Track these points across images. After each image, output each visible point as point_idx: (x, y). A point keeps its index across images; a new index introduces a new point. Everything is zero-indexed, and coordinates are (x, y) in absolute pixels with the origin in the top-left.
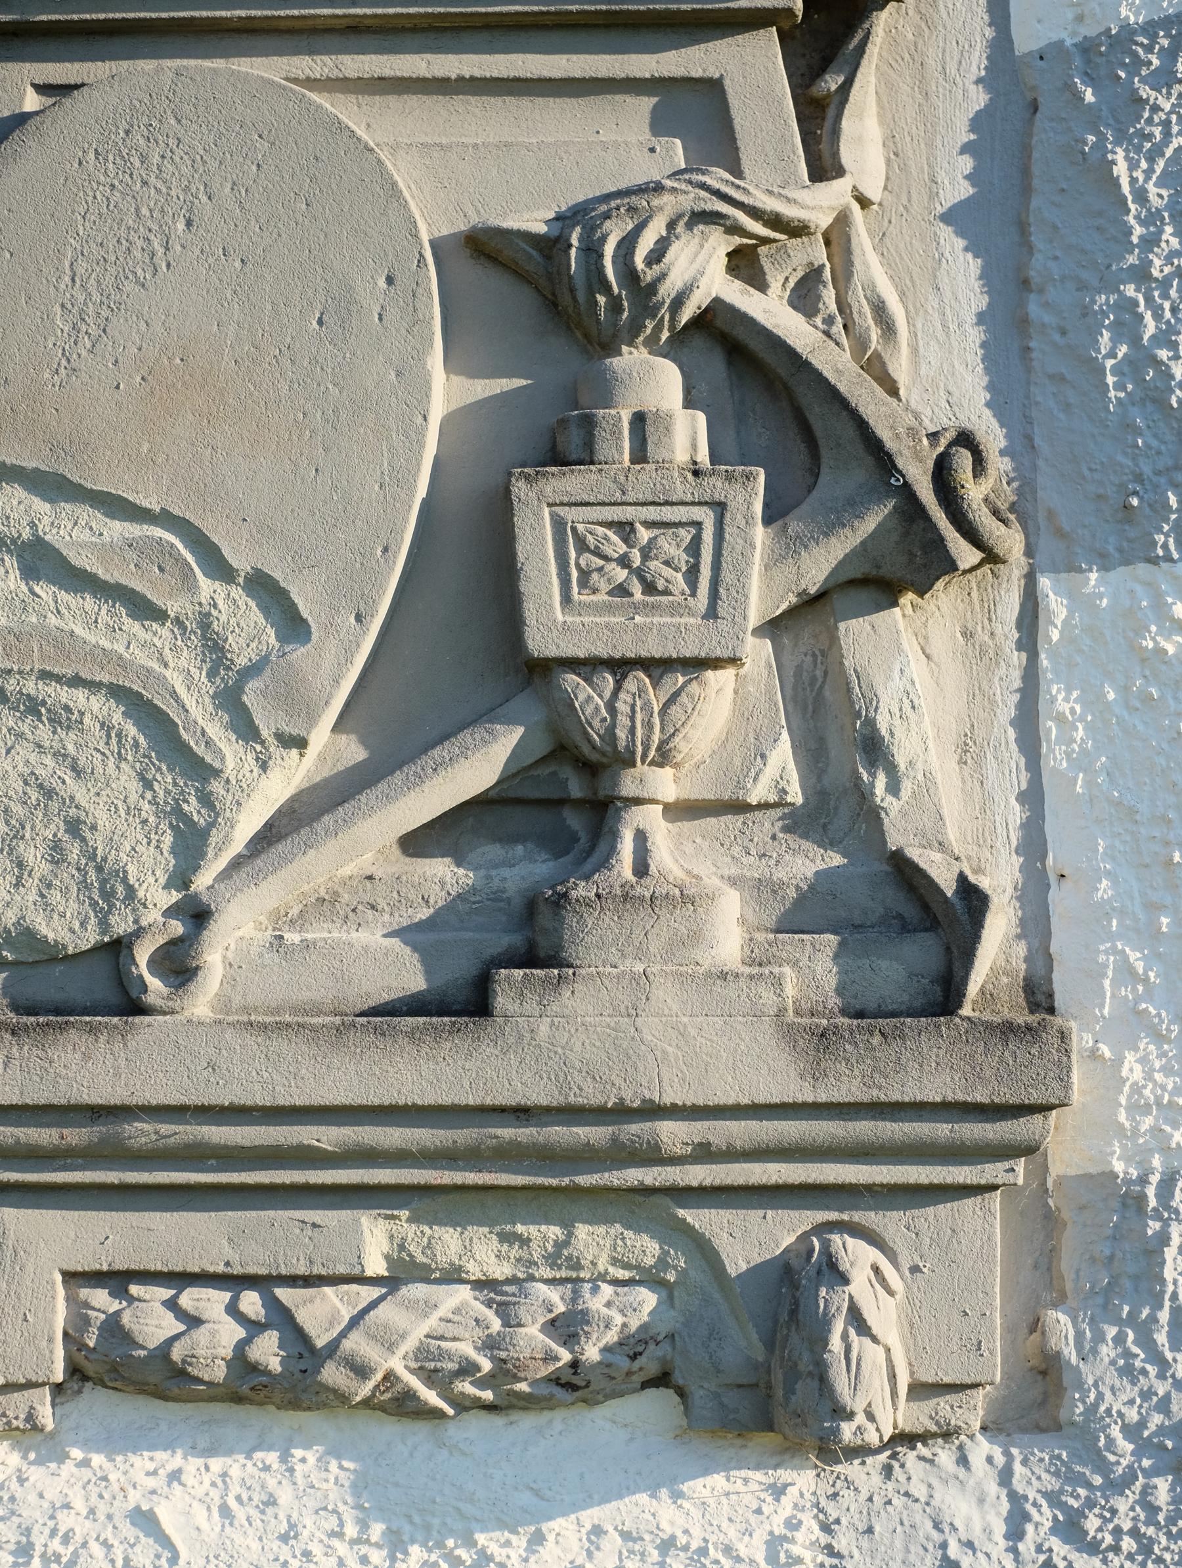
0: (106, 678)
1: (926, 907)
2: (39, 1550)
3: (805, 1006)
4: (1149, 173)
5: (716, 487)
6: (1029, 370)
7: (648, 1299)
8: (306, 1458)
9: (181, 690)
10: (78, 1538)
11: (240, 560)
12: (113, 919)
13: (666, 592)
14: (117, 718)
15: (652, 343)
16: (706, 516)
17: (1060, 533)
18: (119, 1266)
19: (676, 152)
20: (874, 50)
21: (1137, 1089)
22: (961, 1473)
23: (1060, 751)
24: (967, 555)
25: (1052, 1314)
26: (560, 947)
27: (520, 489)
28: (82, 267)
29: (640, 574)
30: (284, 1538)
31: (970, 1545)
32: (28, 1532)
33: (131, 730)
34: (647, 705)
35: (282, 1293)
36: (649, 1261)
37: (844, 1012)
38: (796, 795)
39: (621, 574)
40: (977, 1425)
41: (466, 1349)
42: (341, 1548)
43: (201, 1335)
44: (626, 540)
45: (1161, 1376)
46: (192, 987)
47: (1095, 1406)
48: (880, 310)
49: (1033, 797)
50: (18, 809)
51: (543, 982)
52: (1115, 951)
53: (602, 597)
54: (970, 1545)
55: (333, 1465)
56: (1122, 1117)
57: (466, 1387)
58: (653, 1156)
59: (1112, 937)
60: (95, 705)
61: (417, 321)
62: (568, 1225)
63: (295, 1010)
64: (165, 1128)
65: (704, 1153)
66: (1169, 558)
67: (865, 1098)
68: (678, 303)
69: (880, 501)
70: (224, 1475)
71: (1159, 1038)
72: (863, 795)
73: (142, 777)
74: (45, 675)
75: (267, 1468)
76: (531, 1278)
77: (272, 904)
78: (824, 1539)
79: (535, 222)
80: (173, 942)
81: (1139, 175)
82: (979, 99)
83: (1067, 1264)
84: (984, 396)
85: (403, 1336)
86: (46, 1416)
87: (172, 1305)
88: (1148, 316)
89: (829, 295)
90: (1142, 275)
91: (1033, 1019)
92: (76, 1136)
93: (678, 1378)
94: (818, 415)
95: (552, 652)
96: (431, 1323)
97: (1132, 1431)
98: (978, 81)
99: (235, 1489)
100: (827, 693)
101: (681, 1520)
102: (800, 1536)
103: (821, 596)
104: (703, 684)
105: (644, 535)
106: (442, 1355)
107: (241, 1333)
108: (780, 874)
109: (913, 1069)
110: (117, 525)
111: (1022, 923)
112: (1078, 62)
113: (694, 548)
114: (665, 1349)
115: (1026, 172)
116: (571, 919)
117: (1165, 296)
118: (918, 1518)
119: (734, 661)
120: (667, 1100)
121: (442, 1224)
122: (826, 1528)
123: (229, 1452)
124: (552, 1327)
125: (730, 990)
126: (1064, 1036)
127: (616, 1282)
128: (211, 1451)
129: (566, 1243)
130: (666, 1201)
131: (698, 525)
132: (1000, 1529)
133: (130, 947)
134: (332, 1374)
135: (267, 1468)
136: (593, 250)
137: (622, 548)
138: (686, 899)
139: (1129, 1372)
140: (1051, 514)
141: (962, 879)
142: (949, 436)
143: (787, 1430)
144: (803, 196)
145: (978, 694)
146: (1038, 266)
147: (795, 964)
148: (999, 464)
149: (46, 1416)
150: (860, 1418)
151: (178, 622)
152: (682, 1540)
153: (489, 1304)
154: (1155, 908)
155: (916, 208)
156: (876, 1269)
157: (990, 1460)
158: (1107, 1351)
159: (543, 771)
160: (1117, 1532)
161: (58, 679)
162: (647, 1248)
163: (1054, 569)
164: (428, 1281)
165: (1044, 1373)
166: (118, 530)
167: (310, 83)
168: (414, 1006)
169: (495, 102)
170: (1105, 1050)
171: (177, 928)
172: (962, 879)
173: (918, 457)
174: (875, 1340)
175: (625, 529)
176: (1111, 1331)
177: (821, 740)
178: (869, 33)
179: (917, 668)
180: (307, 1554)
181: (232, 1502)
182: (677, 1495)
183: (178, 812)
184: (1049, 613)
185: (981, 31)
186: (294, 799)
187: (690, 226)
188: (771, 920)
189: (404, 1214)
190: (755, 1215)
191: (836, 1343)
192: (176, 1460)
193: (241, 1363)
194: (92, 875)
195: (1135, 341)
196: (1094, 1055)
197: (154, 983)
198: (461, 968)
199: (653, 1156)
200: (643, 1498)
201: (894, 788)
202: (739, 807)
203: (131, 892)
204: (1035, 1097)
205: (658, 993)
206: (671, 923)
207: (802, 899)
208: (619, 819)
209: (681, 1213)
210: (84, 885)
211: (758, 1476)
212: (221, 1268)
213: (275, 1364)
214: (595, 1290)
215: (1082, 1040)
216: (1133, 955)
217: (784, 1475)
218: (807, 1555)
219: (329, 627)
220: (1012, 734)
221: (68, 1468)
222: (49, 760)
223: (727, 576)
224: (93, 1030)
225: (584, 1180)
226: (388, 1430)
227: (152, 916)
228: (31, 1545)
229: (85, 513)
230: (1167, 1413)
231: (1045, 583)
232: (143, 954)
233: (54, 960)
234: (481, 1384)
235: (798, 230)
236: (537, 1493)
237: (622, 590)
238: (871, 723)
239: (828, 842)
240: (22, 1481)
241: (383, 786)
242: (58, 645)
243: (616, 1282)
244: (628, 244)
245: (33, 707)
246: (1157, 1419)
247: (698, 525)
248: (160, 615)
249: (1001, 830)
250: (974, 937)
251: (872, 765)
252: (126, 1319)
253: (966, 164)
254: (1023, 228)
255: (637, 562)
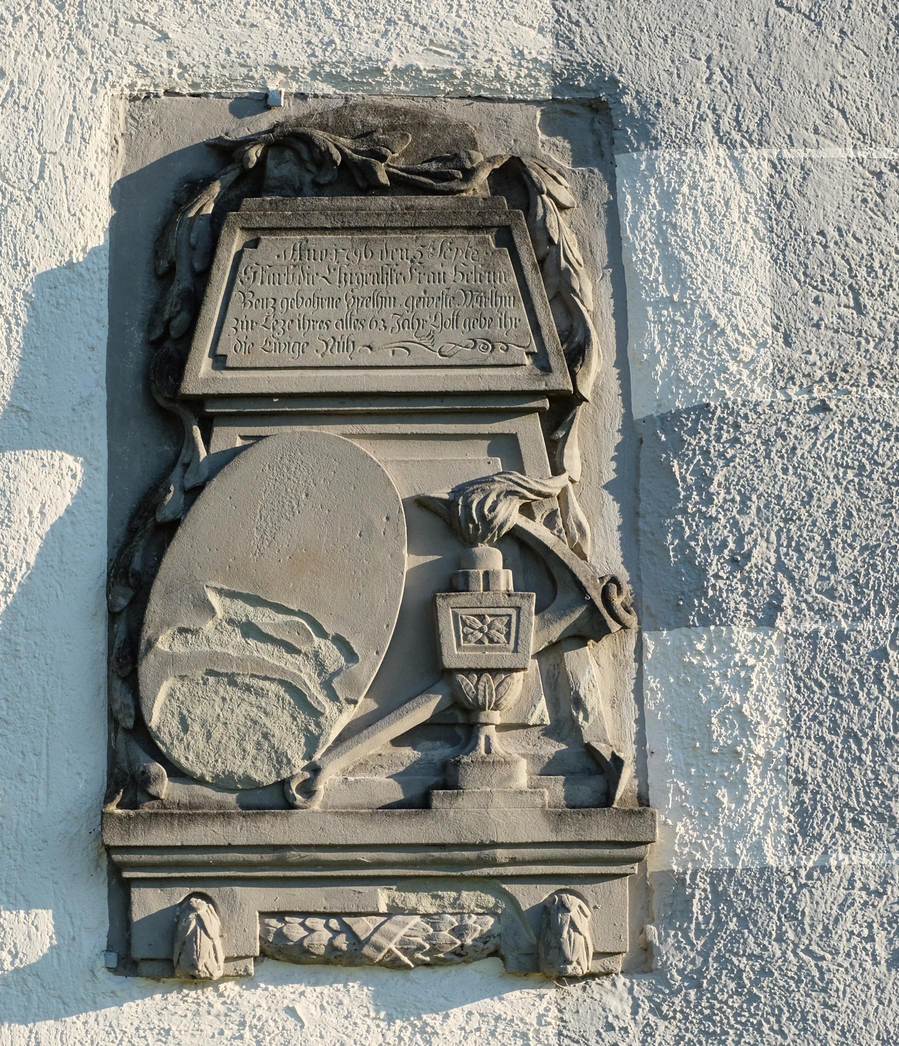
0: (277, 677)
1: (599, 765)
2: (248, 1023)
3: (552, 804)
4: (687, 470)
5: (517, 601)
6: (639, 549)
7: (490, 920)
8: (354, 986)
9: (308, 682)
10: (264, 1019)
11: (330, 630)
12: (282, 772)
13: (498, 642)
14: (282, 692)
15: (490, 543)
16: (513, 612)
17: (651, 615)
18: (281, 909)
19: (498, 464)
20: (577, 421)
21: (682, 837)
22: (613, 989)
23: (651, 703)
24: (615, 627)
25: (649, 926)
26: (457, 781)
27: (440, 601)
28: (264, 513)
29: (487, 635)
30: (346, 1017)
31: (617, 1017)
32: (244, 1017)
33: (287, 697)
34: (490, 686)
35: (346, 920)
36: (491, 905)
37: (567, 806)
38: (547, 721)
39: (480, 635)
40: (620, 970)
41: (420, 940)
42: (369, 1021)
43: (315, 936)
44: (482, 622)
45: (692, 950)
46: (314, 798)
47: (666, 962)
48: (580, 526)
49: (641, 721)
50: (243, 729)
51: (451, 795)
52: (673, 782)
53: (473, 644)
54: (617, 1017)
55: (365, 989)
56: (676, 848)
57: (419, 955)
58: (493, 863)
59: (672, 777)
60: (273, 688)
61: (399, 535)
62: (459, 892)
63: (352, 807)
64: (303, 854)
65: (513, 862)
66: (694, 625)
67: (576, 839)
68: (501, 527)
69: (581, 606)
70: (322, 993)
71: (691, 817)
72: (574, 721)
73: (292, 716)
74: (253, 676)
75: (338, 990)
76: (444, 913)
77: (344, 765)
78: (560, 1015)
79: (443, 493)
80: (305, 781)
81: (683, 471)
82: (619, 438)
83: (655, 907)
84: (621, 560)
85: (395, 935)
86: (252, 969)
87: (303, 924)
88: (687, 528)
89: (560, 521)
90: (684, 511)
91: (641, 809)
92: (267, 857)
93: (502, 952)
94: (556, 571)
95: (453, 666)
96: (405, 930)
97: (680, 972)
98: (618, 431)
99: (326, 999)
100: (559, 680)
101: (503, 1009)
102: (550, 1014)
103: (558, 642)
104: (512, 678)
105: (489, 620)
106: (410, 942)
107: (331, 935)
108: (542, 753)
109: (595, 828)
110: (280, 616)
111: (636, 771)
112: (659, 424)
113: (508, 625)
114: (497, 940)
115: (638, 468)
116: (462, 771)
117: (693, 520)
118: (596, 1007)
119: (524, 669)
120: (500, 841)
121: (409, 892)
122: (560, 1011)
123: (323, 984)
124: (453, 931)
125: (524, 798)
126: (653, 815)
127: (478, 914)
128: (316, 984)
129: (458, 899)
130: (497, 881)
131: (510, 616)
132: (629, 1011)
133: (289, 783)
134: (367, 950)
135: (338, 990)
136: (467, 506)
137: (480, 625)
138: (507, 763)
139: (679, 949)
140: (648, 608)
141: (613, 754)
142: (608, 578)
143: (546, 970)
144: (548, 482)
145: (619, 680)
146: (643, 507)
147: (548, 788)
148: (627, 588)
149: (252, 969)
150: (575, 964)
151: (305, 654)
152: (504, 1016)
153: (427, 923)
154: (689, 765)
155: (593, 483)
156: (580, 907)
157: (624, 984)
158: (670, 940)
159: (449, 712)
160: (675, 1011)
161: (258, 677)
162: (490, 900)
163: (649, 629)
164: (403, 914)
165: (646, 950)
166: (281, 618)
167: (351, 436)
168: (399, 805)
169: (425, 442)
170: (670, 822)
171: (307, 775)
172: (613, 754)
173: (596, 588)
174: (580, 934)
175: (481, 618)
176: (672, 933)
177: (558, 699)
178: (575, 415)
179: (595, 670)
180: (355, 1024)
181: (325, 1004)
182: (501, 999)
183: (307, 729)
184: (647, 647)
185: (619, 410)
186: (349, 724)
187: (505, 496)
188: (538, 770)
189: (394, 887)
190: (533, 887)
191: (565, 935)
192: (302, 988)
193: (331, 947)
194: (273, 755)
195: (681, 538)
196: (665, 823)
197: (298, 797)
198: (417, 790)
199: (493, 863)
200: (488, 1000)
201: (586, 718)
202: (525, 726)
203: (289, 761)
204: (642, 838)
205: (496, 799)
206: (501, 772)
207: (551, 762)
208: (478, 731)
209: (504, 886)
210: (270, 758)
211: (533, 991)
212: (322, 910)
213: (344, 947)
214: (470, 917)
215: (660, 817)
216: (681, 784)
217: (543, 991)
218: (553, 1022)
219: (366, 657)
220: (632, 696)
221: (259, 991)
222: (255, 709)
223: (521, 636)
224: (275, 815)
225: (466, 873)
226: (386, 975)
227: (297, 770)
228: (245, 1022)
229: (267, 611)
230: (694, 964)
231: (645, 635)
232: (294, 785)
233: (258, 788)
234: (425, 954)
235: (547, 496)
236: (446, 999)
237: (480, 642)
238: (577, 693)
239: (560, 740)
240: (241, 996)
241: (386, 719)
242: (258, 664)
243: (478, 914)
244: (481, 504)
245: (248, 688)
246: (690, 967)
247: (510, 616)
248: (298, 652)
249: (628, 735)
250: (618, 777)
251: (577, 710)
252: (285, 930)
253: (613, 465)
254: (636, 491)
255: (486, 630)
